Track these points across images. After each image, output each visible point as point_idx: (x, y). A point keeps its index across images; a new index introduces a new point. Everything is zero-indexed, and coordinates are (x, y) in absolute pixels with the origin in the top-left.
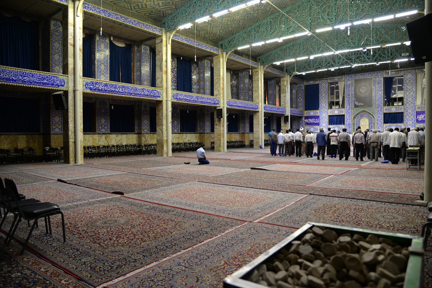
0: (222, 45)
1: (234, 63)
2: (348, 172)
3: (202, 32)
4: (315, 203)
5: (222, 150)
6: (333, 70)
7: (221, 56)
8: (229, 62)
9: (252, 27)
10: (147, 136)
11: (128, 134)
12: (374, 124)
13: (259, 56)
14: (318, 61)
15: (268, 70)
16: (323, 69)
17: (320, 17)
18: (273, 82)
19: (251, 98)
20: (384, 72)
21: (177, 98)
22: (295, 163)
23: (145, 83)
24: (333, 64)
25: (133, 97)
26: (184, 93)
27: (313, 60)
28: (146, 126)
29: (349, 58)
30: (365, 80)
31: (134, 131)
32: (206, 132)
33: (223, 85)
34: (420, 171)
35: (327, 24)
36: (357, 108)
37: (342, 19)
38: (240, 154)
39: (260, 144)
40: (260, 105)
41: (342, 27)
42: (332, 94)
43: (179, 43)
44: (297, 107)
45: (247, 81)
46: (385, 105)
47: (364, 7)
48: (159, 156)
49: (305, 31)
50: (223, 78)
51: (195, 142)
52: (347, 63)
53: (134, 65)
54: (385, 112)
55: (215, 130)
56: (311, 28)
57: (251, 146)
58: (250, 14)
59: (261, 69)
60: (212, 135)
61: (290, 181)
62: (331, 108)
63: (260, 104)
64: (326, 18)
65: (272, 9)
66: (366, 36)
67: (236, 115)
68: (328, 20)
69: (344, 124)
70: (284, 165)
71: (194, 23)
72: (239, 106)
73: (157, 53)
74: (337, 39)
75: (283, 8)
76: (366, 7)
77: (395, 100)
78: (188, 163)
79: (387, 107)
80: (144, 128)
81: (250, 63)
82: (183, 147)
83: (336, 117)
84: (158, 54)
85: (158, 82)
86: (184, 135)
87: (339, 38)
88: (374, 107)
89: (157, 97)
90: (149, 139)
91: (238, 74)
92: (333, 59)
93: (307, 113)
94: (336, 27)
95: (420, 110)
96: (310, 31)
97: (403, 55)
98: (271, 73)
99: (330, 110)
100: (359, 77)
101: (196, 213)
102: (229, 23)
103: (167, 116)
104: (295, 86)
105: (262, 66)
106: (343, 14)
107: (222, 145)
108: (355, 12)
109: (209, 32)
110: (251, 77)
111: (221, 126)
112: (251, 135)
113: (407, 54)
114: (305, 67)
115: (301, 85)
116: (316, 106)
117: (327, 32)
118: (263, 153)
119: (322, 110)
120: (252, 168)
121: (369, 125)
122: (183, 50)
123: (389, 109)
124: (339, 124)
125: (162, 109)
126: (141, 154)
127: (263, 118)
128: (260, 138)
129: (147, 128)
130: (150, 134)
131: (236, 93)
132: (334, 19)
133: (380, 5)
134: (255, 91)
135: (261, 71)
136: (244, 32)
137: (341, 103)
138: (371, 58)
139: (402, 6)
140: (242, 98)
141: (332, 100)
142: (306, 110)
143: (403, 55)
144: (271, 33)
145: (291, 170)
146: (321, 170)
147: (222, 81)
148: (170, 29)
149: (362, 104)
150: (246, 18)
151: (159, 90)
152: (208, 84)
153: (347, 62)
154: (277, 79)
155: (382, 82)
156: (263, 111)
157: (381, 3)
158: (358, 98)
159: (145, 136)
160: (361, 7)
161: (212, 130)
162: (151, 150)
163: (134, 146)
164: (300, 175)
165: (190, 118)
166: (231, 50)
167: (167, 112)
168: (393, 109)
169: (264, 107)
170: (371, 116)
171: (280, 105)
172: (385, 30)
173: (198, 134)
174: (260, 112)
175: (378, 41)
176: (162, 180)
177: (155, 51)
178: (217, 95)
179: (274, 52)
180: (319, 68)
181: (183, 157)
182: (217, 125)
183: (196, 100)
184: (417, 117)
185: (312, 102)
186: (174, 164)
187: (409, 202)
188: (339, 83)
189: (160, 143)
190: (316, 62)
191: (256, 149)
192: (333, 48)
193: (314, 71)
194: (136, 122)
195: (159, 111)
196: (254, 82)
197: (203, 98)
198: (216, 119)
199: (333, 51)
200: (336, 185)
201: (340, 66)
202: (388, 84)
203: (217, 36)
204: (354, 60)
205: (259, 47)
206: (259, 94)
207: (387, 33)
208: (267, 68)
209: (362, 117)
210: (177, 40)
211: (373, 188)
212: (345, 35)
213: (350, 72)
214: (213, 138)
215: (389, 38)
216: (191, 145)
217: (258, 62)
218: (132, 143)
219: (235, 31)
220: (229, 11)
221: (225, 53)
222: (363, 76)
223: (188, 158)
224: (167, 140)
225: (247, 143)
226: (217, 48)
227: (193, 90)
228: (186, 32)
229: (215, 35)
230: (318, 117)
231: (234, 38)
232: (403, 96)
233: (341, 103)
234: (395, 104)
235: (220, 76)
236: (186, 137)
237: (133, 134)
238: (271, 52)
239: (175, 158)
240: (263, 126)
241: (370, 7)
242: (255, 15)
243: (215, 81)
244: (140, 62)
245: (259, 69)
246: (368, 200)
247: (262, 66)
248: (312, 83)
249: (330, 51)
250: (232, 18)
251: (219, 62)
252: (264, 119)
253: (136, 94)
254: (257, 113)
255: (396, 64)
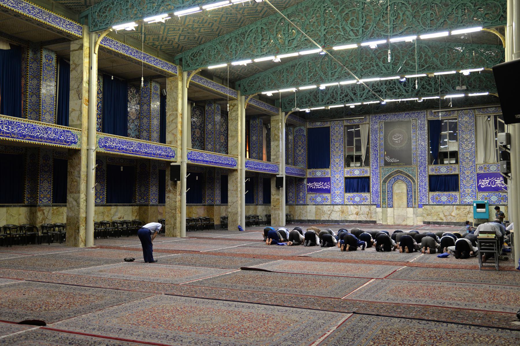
0: (181, 60)
1: (198, 89)
2: (395, 274)
3: (150, 36)
4: (366, 327)
5: (178, 234)
6: (353, 107)
7: (180, 78)
8: (192, 88)
9: (232, 35)
10: (46, 209)
11: (10, 206)
12: (415, 192)
13: (240, 79)
14: (330, 92)
15: (251, 103)
16: (337, 104)
17: (340, 27)
18: (258, 121)
19: (225, 149)
20: (428, 113)
21: (105, 146)
22: (307, 258)
23: (48, 117)
24: (353, 97)
25: (27, 141)
26: (118, 138)
27: (322, 91)
28: (45, 193)
29: (377, 90)
30: (400, 123)
31: (23, 202)
32: (151, 203)
33: (182, 126)
34: (500, 272)
35: (349, 39)
36: (389, 167)
37: (373, 33)
38: (211, 241)
39: (239, 223)
40: (239, 159)
41: (373, 44)
42: (350, 143)
43: (110, 52)
44: (295, 163)
45: (218, 118)
46: (430, 163)
47: (406, 17)
48: (70, 246)
49: (316, 47)
50: (182, 114)
51: (131, 220)
52: (374, 97)
53: (26, 84)
54: (431, 173)
55: (167, 200)
56: (325, 43)
57: (224, 226)
58: (231, 14)
59: (241, 100)
60: (160, 209)
61: (313, 291)
62: (348, 165)
63: (239, 157)
64: (348, 29)
65: (265, 9)
66: (405, 58)
67: (199, 175)
68: (351, 33)
69: (369, 191)
70: (291, 262)
71: (141, 23)
72: (207, 161)
73: (72, 67)
74: (365, 61)
75: (283, 8)
76: (409, 16)
77: (445, 155)
78: (132, 260)
79: (433, 166)
80: (42, 196)
81: (226, 91)
82: (110, 228)
83: (356, 180)
84: (74, 69)
85: (73, 116)
86: (113, 209)
87: (364, 59)
88: (414, 166)
89: (72, 143)
90: (50, 216)
91: (204, 108)
92: (352, 90)
93: (310, 173)
94: (363, 44)
95: (482, 172)
96: (324, 47)
97: (458, 88)
98: (257, 108)
99: (347, 169)
100: (391, 118)
101: (89, 338)
102: (196, 25)
103: (87, 176)
104: (291, 129)
105: (243, 97)
106: (375, 25)
107: (178, 225)
108: (392, 23)
109: (161, 38)
110: (225, 114)
111: (178, 193)
112: (223, 208)
113: (464, 87)
114: (309, 100)
115: (302, 128)
116: (325, 163)
117: (353, 50)
118: (252, 240)
119: (335, 169)
120: (243, 269)
121: (408, 194)
122: (115, 64)
123: (436, 170)
124: (361, 192)
125: (79, 163)
126: (33, 243)
127: (244, 181)
128: (239, 213)
129: (48, 196)
130: (53, 206)
131: (199, 140)
132: (361, 31)
133: (429, 15)
134: (232, 136)
135: (241, 105)
136: (218, 41)
137: (363, 158)
138: (410, 90)
139: (460, 19)
140: (209, 147)
141: (351, 154)
142: (309, 168)
143: (458, 88)
144: (262, 46)
145: (305, 271)
146: (352, 270)
147: (179, 120)
148: (96, 29)
149: (396, 161)
150: (223, 19)
151: (74, 132)
152: (156, 122)
153: (375, 95)
154: (264, 117)
155: (426, 128)
156: (244, 169)
157: (431, 12)
158: (390, 152)
159: (43, 210)
160: (401, 15)
161: (162, 200)
162: (53, 236)
163: (21, 228)
164: (324, 279)
165: (123, 179)
166: (196, 69)
167: (88, 169)
168: (443, 170)
169: (246, 164)
170: (409, 179)
171: (269, 159)
172: (432, 51)
173: (137, 207)
174: (239, 171)
175: (423, 66)
176: (101, 294)
177: (69, 65)
178: (171, 142)
179: (263, 74)
180: (332, 103)
181: (114, 248)
182: (170, 191)
183: (138, 149)
184: (478, 183)
185: (319, 156)
186: (107, 262)
187: (503, 324)
188: (360, 126)
189: (73, 224)
190: (326, 93)
191: (232, 232)
192: (355, 73)
193: (323, 108)
194: (27, 185)
195: (72, 167)
196: (230, 123)
197: (149, 147)
198: (169, 182)
199: (355, 79)
200: (385, 296)
201: (364, 100)
202: (435, 130)
203: (174, 45)
204: (384, 93)
205: (243, 67)
206: (237, 141)
207: (435, 55)
208: (250, 101)
209: (396, 180)
210: (108, 47)
211: (443, 301)
212: (373, 55)
213: (378, 110)
214: (161, 214)
215: (439, 63)
216: (125, 226)
217: (237, 90)
218: (17, 224)
219: (204, 39)
220: (201, 9)
221: (185, 74)
222: (397, 117)
223: (124, 249)
224: (86, 218)
225: (217, 222)
226: (174, 65)
227: (129, 131)
228: (124, 35)
229: (171, 42)
230: (328, 180)
231: (203, 50)
232: (457, 150)
233: (363, 158)
234: (446, 162)
235: (177, 110)
236: (116, 212)
237: (20, 206)
238: (257, 75)
239: (102, 250)
240: (244, 193)
241: (414, 17)
242: (239, 16)
243: (169, 119)
244: (39, 80)
245: (239, 102)
246: (444, 322)
247: (243, 97)
248: (318, 124)
249: (352, 78)
250: (202, 18)
251: (177, 87)
252: (246, 183)
253: (33, 137)
254: (235, 173)
255: (448, 100)
